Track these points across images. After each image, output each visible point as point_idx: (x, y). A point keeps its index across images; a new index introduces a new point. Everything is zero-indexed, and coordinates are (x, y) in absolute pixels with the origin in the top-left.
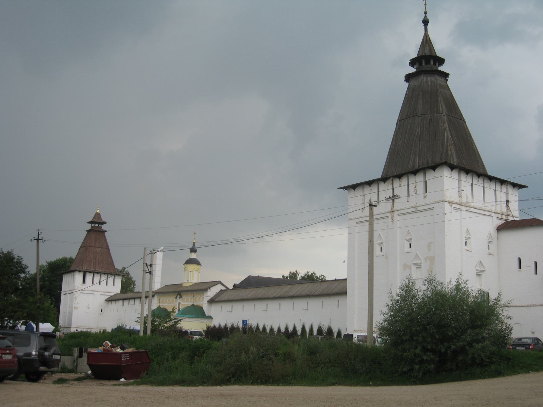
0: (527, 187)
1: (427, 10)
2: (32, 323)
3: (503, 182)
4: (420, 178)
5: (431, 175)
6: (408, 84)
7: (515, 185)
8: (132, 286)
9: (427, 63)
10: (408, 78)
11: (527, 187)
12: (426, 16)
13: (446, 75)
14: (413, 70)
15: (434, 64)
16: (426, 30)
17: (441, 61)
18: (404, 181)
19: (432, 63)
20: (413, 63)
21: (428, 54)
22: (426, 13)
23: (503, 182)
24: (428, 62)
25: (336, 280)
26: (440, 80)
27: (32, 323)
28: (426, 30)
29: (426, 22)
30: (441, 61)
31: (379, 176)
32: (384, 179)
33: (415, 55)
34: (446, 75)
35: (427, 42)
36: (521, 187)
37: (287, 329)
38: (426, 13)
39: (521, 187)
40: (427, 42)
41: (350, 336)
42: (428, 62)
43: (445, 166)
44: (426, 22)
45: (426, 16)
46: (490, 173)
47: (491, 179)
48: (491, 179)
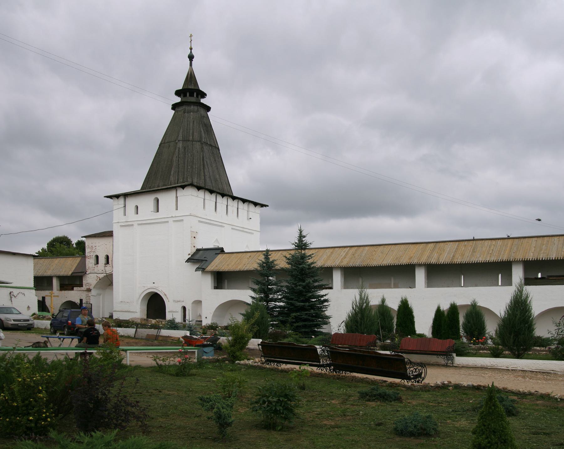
0: (268, 206)
3: (244, 201)
5: (181, 192)
6: (173, 112)
7: (256, 204)
8: (45, 366)
9: (190, 96)
10: (174, 107)
11: (268, 206)
12: (191, 52)
13: (208, 109)
14: (178, 100)
15: (197, 96)
17: (203, 95)
19: (195, 96)
21: (192, 87)
23: (244, 201)
26: (202, 111)
29: (191, 57)
30: (203, 95)
31: (138, 187)
33: (181, 88)
34: (208, 109)
35: (191, 78)
36: (262, 206)
38: (191, 49)
39: (262, 206)
41: (39, 251)
45: (191, 52)
46: (235, 194)
47: (234, 198)
48: (234, 198)
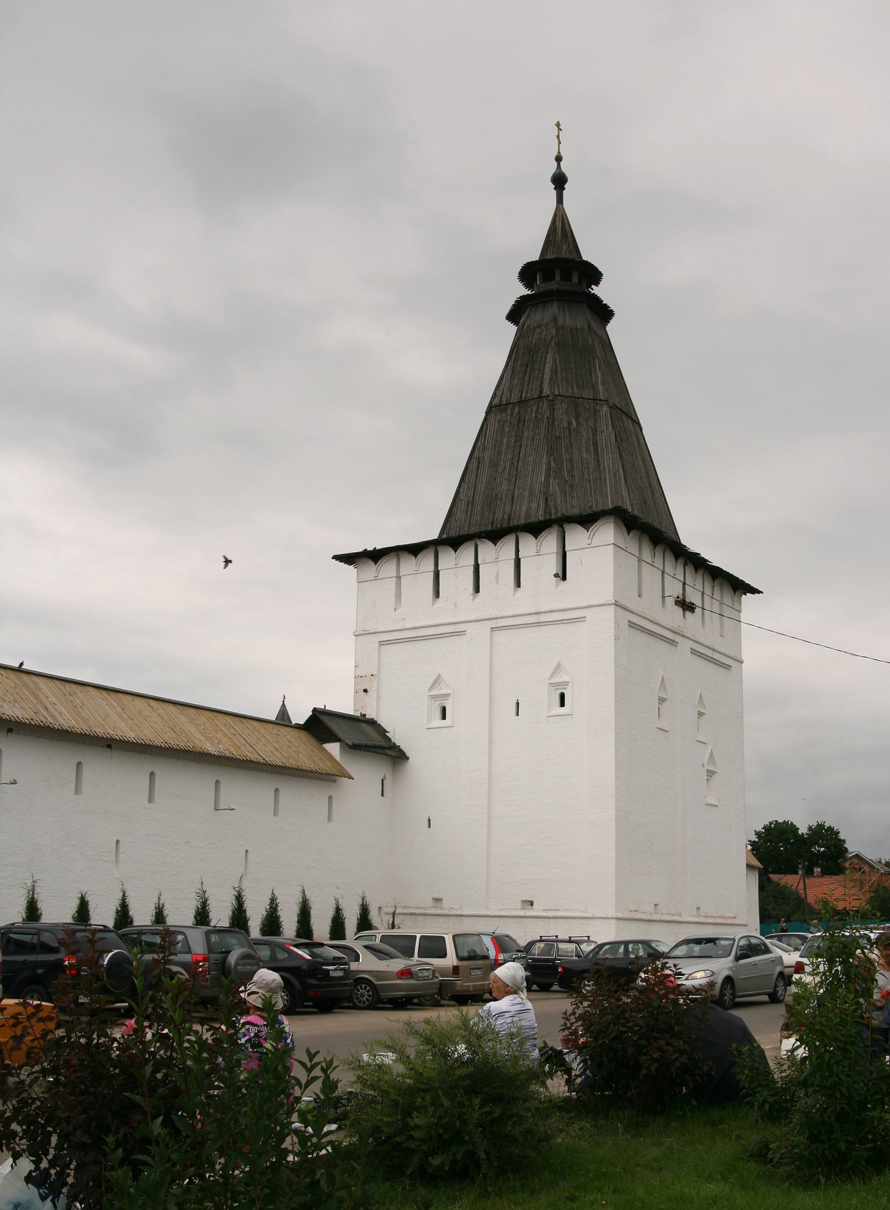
1: (564, 169)
2: (156, 956)
4: (549, 542)
12: (559, 166)
16: (560, 200)
17: (753, 844)
18: (506, 548)
20: (528, 274)
22: (559, 159)
24: (566, 278)
25: (19, 670)
27: (156, 956)
28: (560, 200)
29: (559, 181)
32: (452, 539)
33: (534, 255)
35: (560, 231)
37: (123, 915)
38: (559, 159)
40: (560, 231)
42: (566, 278)
43: (611, 519)
44: (559, 181)
45: (559, 166)
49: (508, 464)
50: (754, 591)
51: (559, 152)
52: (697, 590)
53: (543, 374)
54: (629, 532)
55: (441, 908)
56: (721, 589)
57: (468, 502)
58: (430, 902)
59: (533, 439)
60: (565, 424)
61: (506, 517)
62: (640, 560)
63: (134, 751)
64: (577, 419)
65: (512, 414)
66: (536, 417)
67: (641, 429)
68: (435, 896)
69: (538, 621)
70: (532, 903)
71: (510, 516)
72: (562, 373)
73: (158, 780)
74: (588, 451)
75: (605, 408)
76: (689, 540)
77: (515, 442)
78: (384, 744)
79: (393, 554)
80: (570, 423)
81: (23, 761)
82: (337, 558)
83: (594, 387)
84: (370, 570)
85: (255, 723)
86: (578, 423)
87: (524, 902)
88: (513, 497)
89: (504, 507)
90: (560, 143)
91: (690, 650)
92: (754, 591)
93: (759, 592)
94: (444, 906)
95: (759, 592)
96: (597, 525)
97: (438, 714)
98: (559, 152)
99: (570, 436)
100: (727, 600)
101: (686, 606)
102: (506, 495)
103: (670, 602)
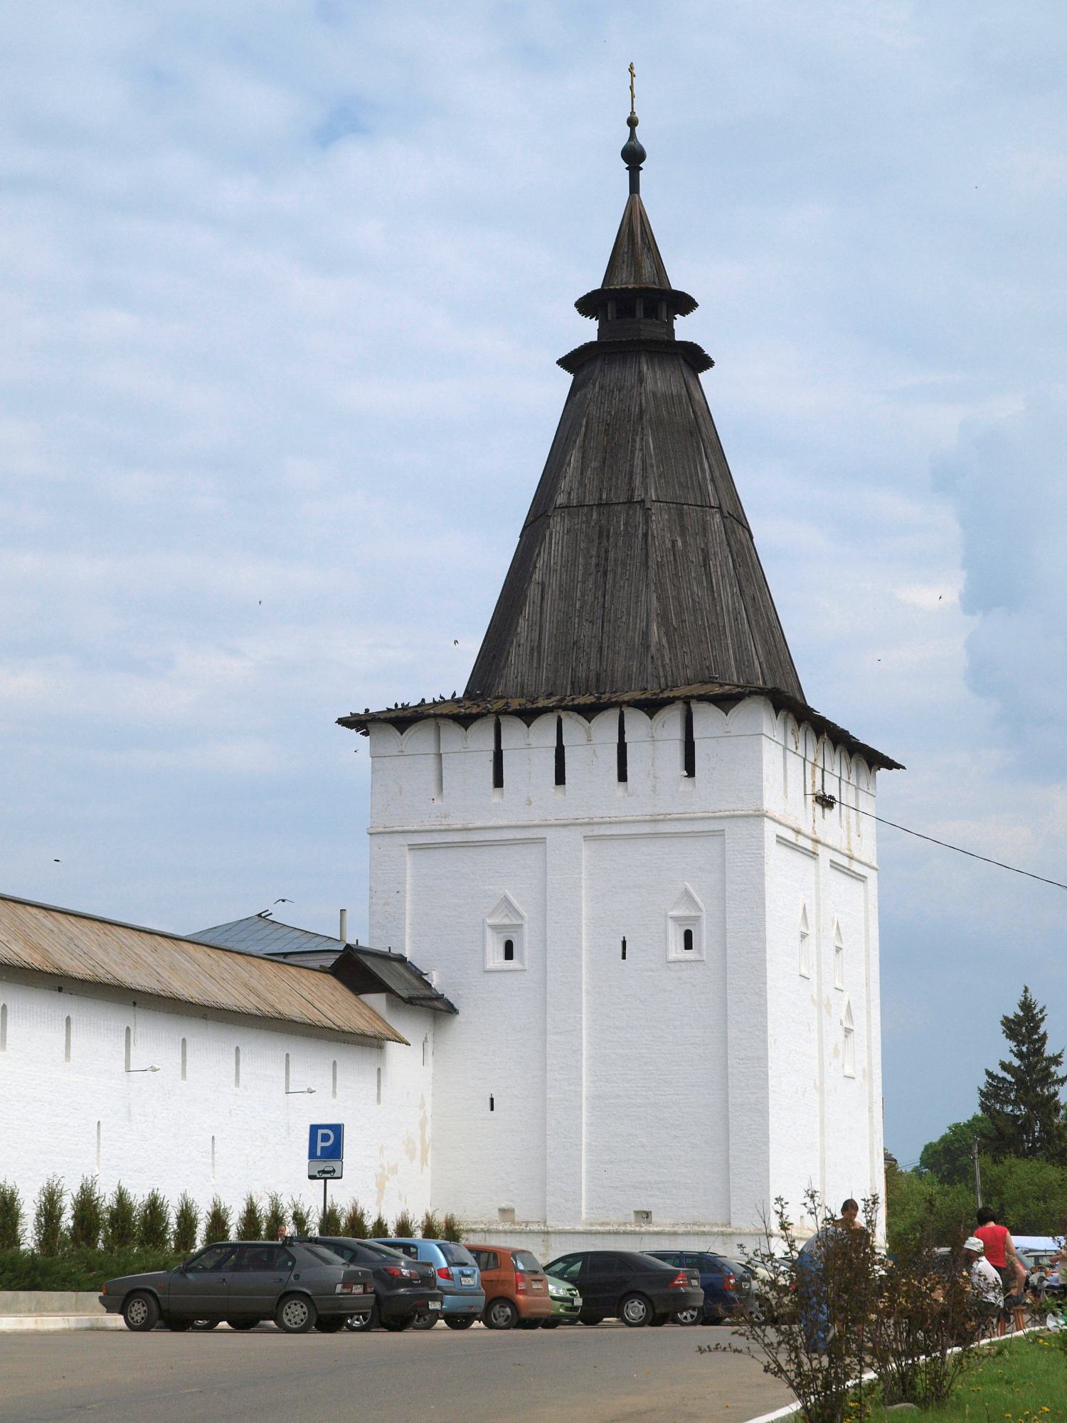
4: (670, 724)
12: (633, 135)
22: (632, 122)
29: (633, 157)
35: (635, 239)
38: (632, 122)
44: (633, 157)
45: (633, 135)
49: (589, 599)
50: (891, 765)
51: (632, 113)
52: (835, 775)
53: (632, 466)
54: (777, 711)
55: (513, 1222)
56: (857, 767)
57: (532, 649)
58: (496, 1215)
59: (624, 564)
60: (669, 545)
61: (593, 675)
62: (785, 748)
63: (205, 1017)
64: (683, 535)
65: (588, 522)
66: (626, 529)
67: (751, 537)
68: (503, 1205)
69: (656, 829)
70: (647, 1215)
71: (598, 675)
72: (658, 467)
73: (73, 1026)
74: (700, 583)
75: (718, 518)
76: (817, 699)
77: (597, 565)
78: (427, 993)
79: (431, 722)
80: (674, 543)
81: (35, 1027)
82: (343, 722)
83: (702, 489)
84: (392, 740)
85: (120, 930)
86: (684, 543)
87: (637, 1213)
88: (601, 648)
89: (588, 661)
90: (633, 96)
91: (828, 863)
92: (891, 765)
93: (898, 766)
94: (517, 1219)
95: (898, 766)
96: (741, 704)
97: (501, 950)
98: (632, 113)
99: (675, 560)
100: (863, 779)
101: (826, 802)
102: (590, 643)
103: (810, 798)
